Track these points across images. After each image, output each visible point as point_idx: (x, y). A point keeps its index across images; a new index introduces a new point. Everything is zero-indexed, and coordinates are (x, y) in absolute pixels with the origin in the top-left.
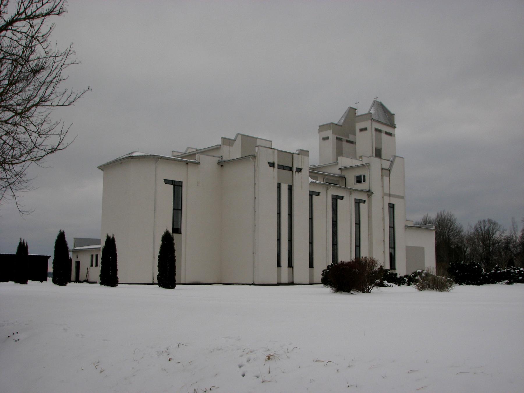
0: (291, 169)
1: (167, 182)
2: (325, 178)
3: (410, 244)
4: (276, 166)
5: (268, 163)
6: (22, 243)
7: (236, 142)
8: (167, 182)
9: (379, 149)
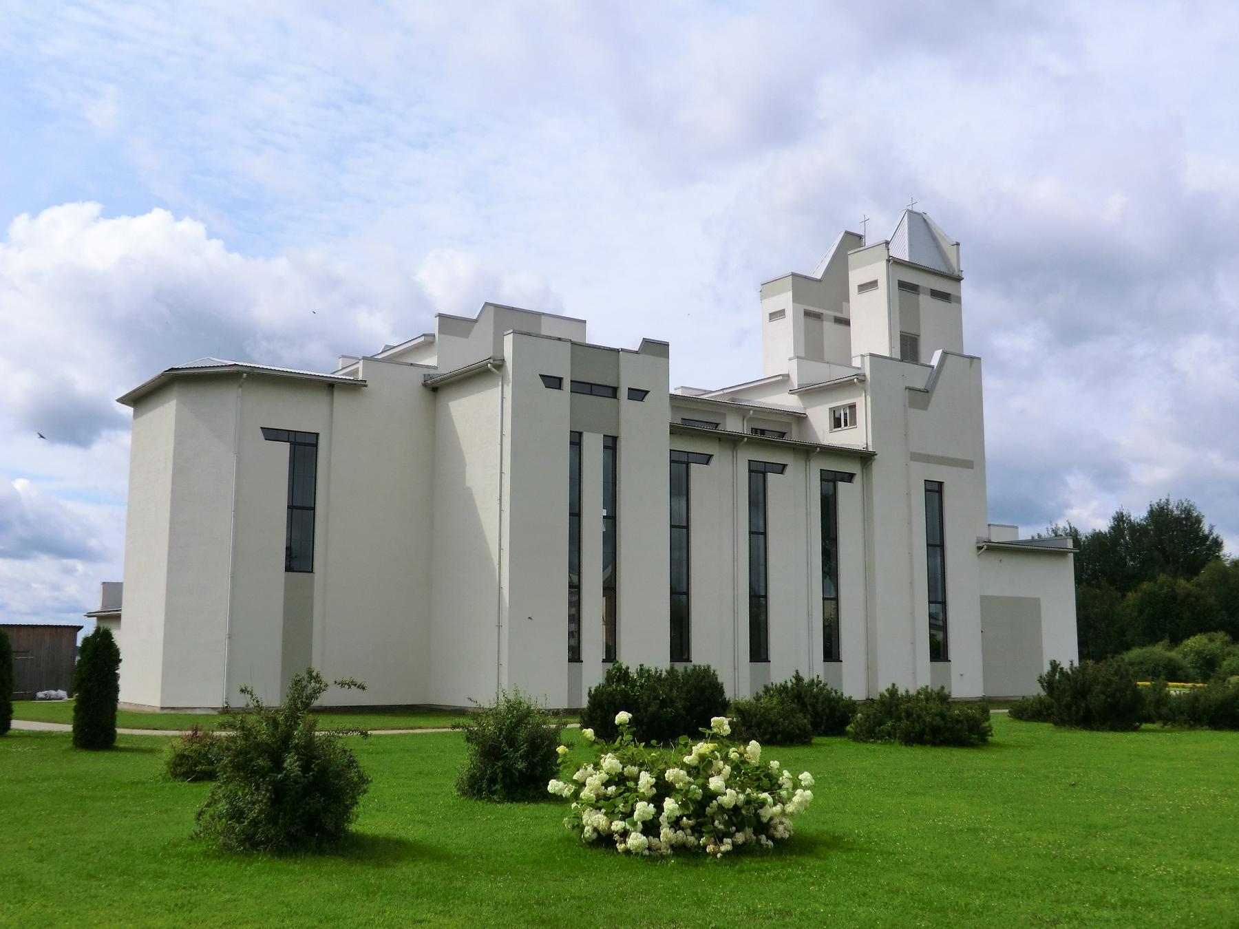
0: (614, 392)
1: (271, 434)
2: (747, 418)
3: (995, 590)
4: (567, 385)
5: (540, 375)
6: (1070, 672)
7: (477, 326)
8: (271, 434)
9: (911, 338)
